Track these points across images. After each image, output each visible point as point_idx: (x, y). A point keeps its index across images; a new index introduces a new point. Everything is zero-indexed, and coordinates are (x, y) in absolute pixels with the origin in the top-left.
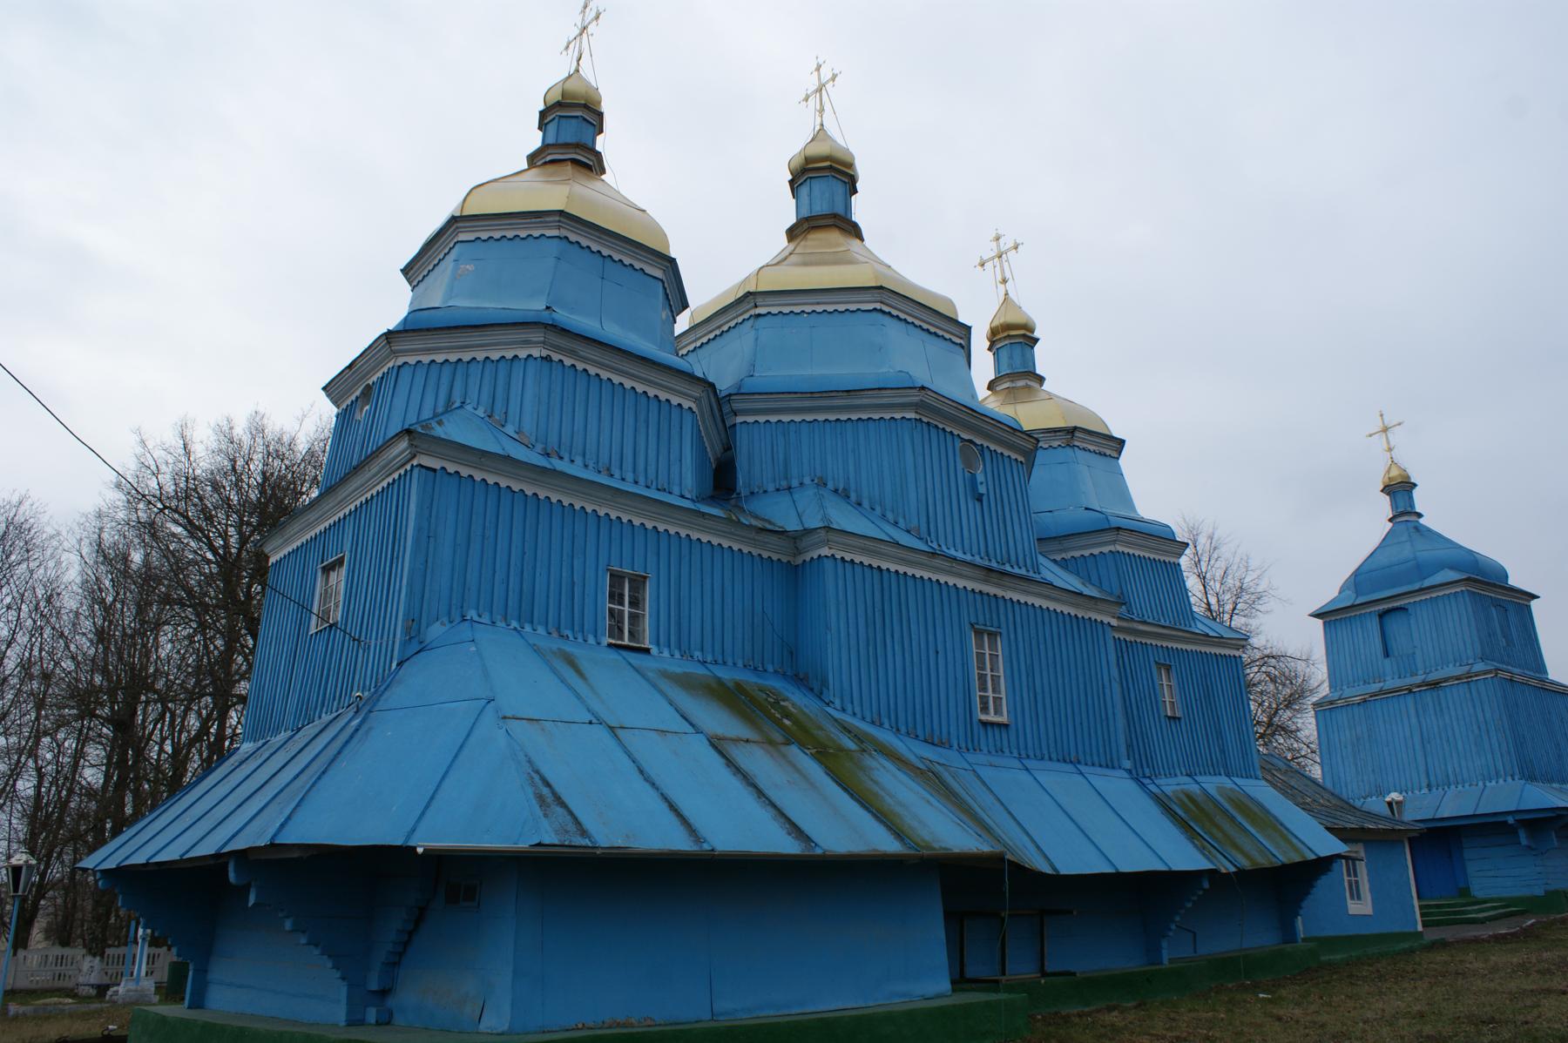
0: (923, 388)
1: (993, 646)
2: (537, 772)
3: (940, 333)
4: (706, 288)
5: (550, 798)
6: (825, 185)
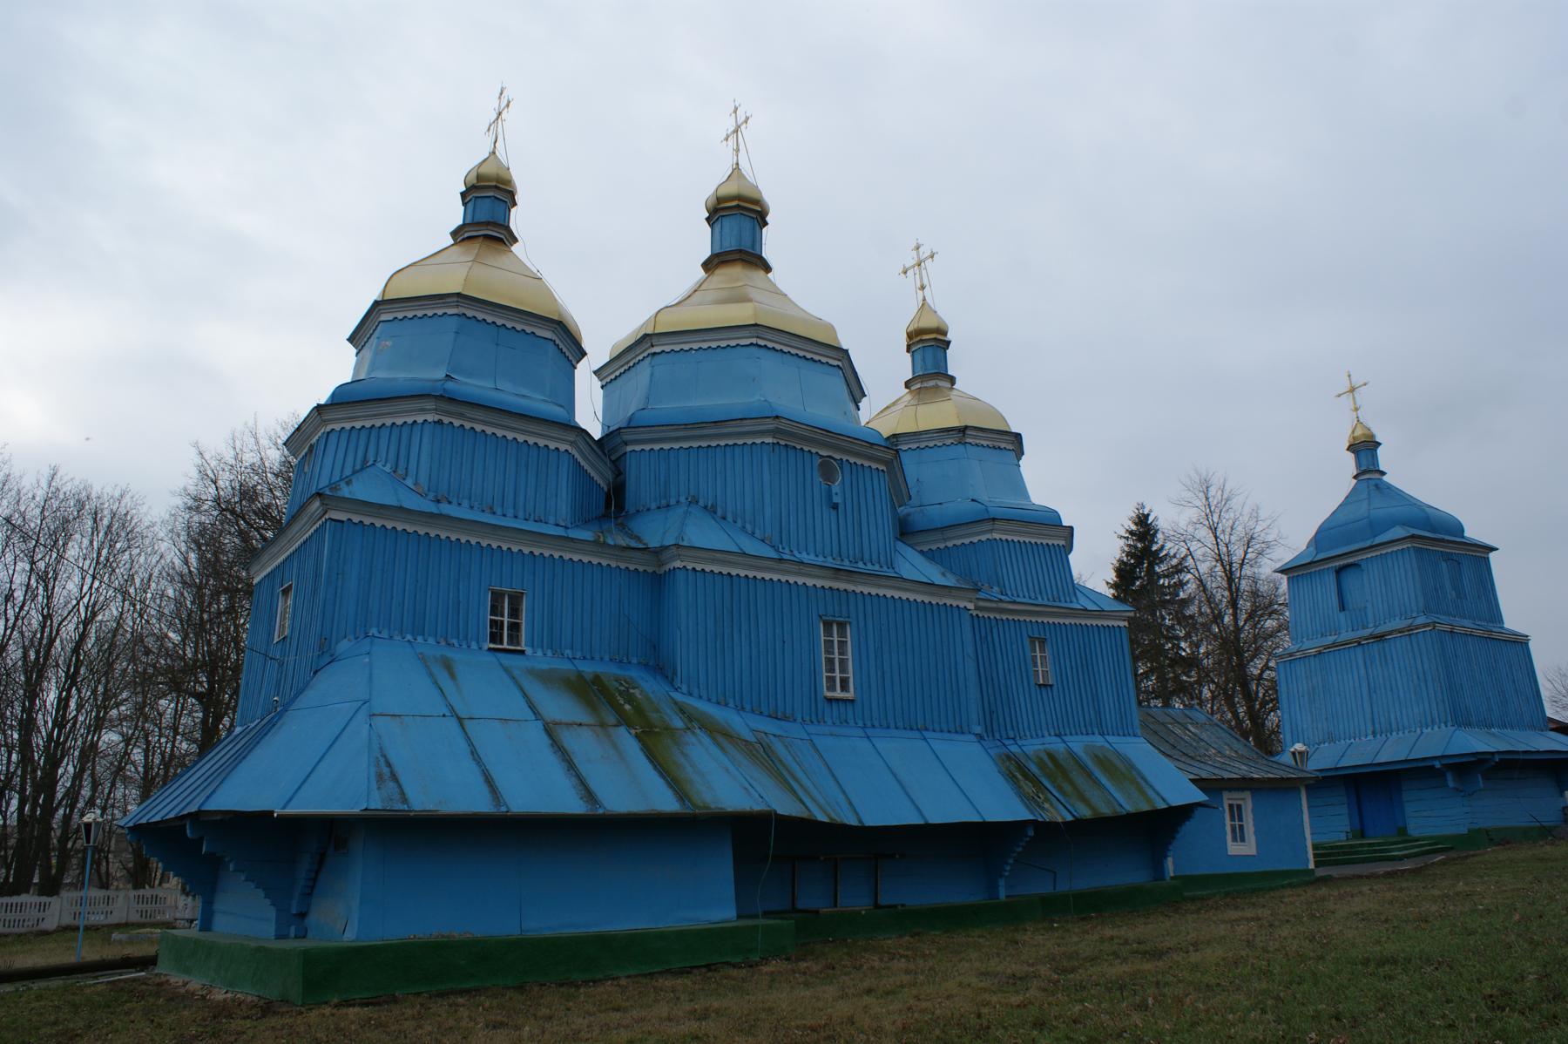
1: (842, 633)
3: (817, 358)
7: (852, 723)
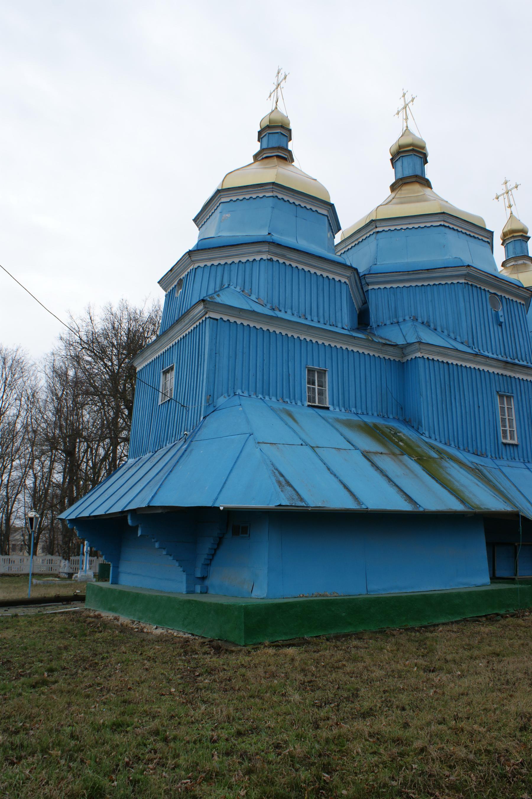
0: (469, 266)
1: (509, 403)
2: (277, 469)
3: (476, 236)
4: (350, 219)
5: (284, 483)
6: (410, 159)
7: (517, 458)
